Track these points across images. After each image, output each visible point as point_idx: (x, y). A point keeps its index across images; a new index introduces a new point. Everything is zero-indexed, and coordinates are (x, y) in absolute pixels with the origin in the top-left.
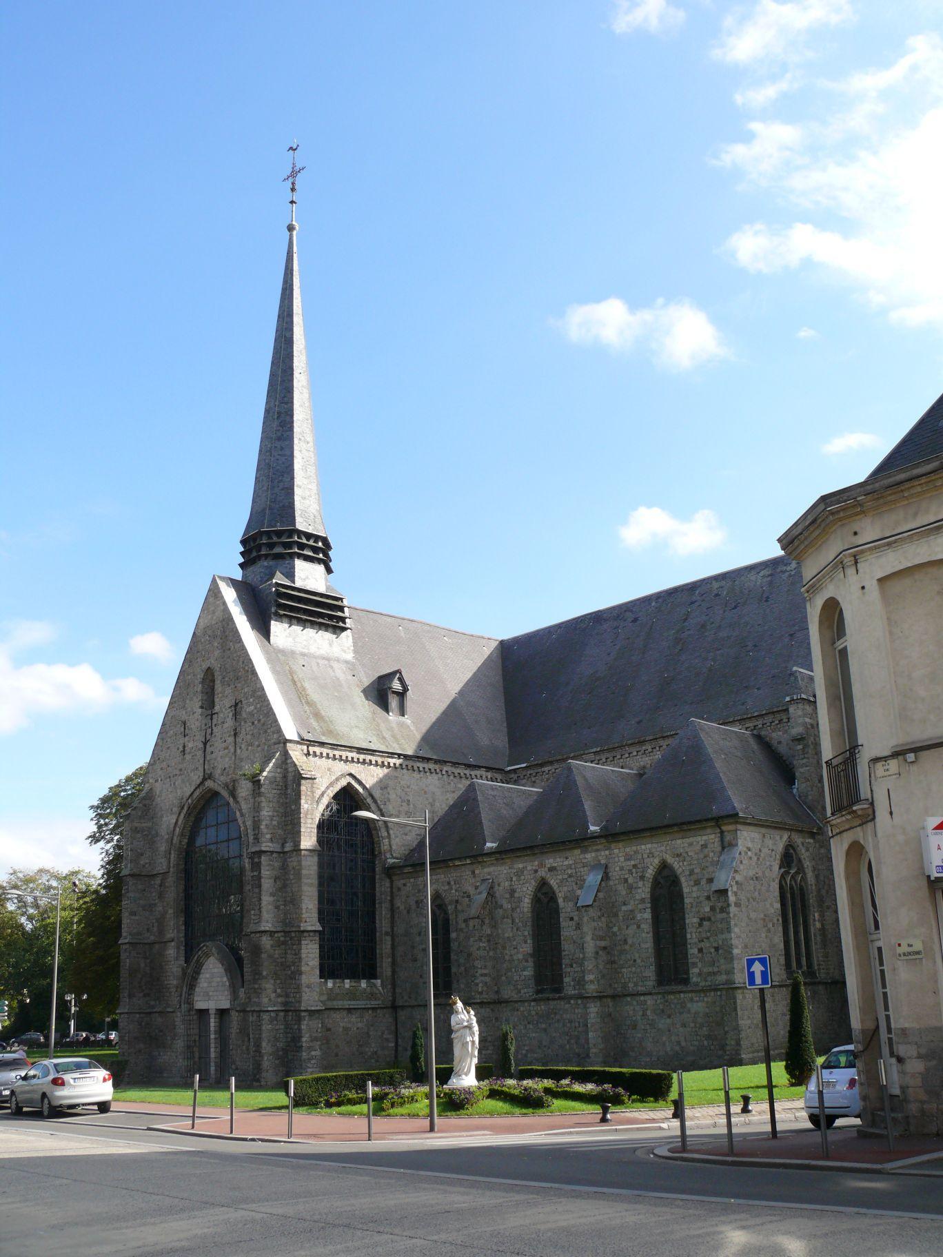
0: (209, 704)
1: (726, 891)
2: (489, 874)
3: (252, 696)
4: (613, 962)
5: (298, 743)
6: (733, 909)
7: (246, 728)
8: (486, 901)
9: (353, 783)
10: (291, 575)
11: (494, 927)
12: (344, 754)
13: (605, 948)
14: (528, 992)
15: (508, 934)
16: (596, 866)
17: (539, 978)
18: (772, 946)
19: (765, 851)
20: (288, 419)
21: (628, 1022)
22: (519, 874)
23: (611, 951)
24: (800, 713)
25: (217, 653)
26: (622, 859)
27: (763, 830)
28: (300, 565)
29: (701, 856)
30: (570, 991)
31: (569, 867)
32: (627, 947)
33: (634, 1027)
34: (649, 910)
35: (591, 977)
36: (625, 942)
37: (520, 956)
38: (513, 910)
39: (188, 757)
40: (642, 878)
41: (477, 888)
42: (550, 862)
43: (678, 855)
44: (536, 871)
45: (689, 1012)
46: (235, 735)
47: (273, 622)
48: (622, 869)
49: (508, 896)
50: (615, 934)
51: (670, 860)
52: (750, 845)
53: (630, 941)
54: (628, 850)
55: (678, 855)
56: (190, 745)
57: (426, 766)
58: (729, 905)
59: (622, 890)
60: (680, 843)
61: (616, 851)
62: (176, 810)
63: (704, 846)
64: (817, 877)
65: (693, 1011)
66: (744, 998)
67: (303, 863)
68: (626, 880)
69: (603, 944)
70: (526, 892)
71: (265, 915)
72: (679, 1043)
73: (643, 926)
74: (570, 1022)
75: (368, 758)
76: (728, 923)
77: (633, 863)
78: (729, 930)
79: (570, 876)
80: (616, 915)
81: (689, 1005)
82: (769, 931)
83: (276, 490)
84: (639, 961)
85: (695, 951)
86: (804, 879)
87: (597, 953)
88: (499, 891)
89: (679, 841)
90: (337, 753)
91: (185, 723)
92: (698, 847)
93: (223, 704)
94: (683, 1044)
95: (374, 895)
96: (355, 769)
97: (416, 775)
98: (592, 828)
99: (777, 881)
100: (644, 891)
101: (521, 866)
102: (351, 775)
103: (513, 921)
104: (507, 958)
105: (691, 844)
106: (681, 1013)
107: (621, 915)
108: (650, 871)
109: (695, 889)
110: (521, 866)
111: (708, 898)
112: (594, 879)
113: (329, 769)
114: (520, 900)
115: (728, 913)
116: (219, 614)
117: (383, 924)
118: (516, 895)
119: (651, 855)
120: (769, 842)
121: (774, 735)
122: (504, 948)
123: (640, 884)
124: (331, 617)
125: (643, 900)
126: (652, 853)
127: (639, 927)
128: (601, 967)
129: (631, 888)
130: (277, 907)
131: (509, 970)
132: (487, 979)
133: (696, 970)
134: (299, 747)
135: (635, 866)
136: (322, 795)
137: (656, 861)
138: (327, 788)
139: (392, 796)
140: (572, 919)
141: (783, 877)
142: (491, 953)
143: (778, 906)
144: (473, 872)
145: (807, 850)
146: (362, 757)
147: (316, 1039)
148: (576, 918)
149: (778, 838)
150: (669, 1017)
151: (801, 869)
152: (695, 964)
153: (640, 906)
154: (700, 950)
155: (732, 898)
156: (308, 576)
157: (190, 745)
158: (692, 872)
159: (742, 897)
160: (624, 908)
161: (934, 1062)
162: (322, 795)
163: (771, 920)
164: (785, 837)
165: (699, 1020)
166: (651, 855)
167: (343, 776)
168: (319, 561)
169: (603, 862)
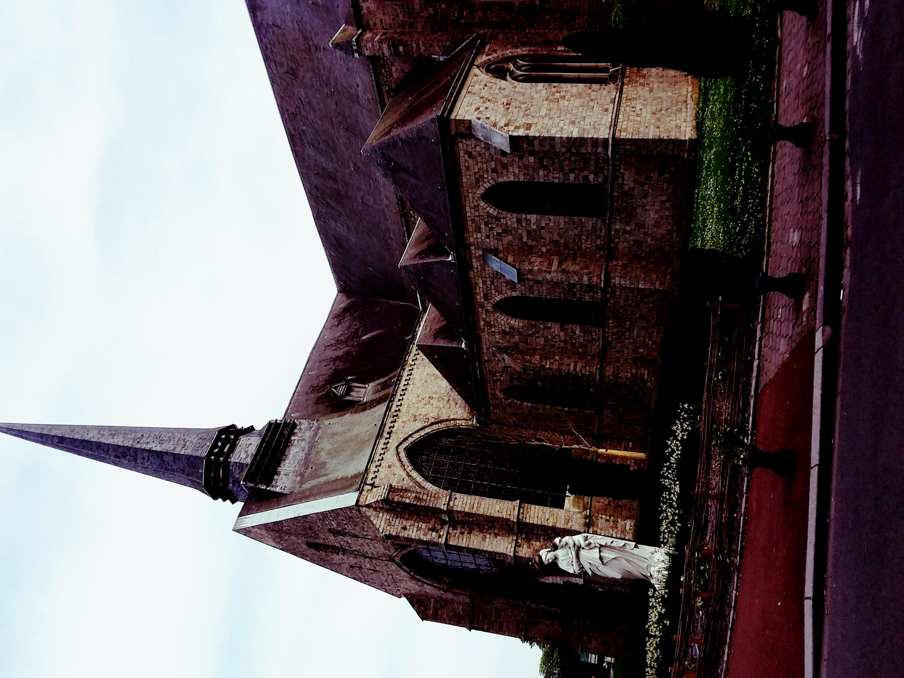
0: (336, 550)
1: (512, 138)
2: (488, 349)
3: (324, 521)
5: (360, 493)
6: (532, 133)
7: (349, 528)
8: (511, 356)
9: (401, 449)
10: (241, 466)
12: (380, 451)
14: (596, 333)
15: (542, 341)
16: (484, 259)
18: (580, 95)
19: (484, 93)
20: (121, 450)
22: (488, 324)
23: (563, 251)
24: (369, 45)
25: (293, 538)
26: (479, 235)
27: (464, 92)
28: (234, 459)
29: (479, 158)
31: (484, 283)
32: (562, 241)
33: (638, 243)
34: (529, 216)
35: (585, 278)
36: (557, 242)
37: (562, 334)
38: (520, 334)
39: (377, 568)
40: (498, 219)
41: (499, 360)
42: (480, 298)
43: (478, 182)
44: (487, 311)
45: (633, 189)
46: (357, 536)
48: (488, 237)
49: (508, 337)
50: (548, 251)
51: (481, 191)
52: (474, 107)
53: (556, 238)
54: (470, 229)
55: (478, 182)
56: (368, 566)
57: (404, 379)
58: (527, 137)
59: (508, 238)
60: (466, 179)
61: (472, 240)
62: (420, 583)
63: (470, 155)
64: (524, 44)
65: (632, 185)
66: (625, 130)
67: (459, 509)
68: (499, 234)
70: (504, 321)
71: (501, 549)
72: (663, 202)
73: (543, 224)
74: (627, 299)
75: (387, 429)
76: (545, 138)
77: (483, 226)
78: (552, 139)
79: (493, 283)
80: (531, 247)
81: (626, 188)
82: (563, 97)
83: (175, 467)
84: (576, 232)
85: (572, 176)
86: (522, 57)
88: (503, 343)
89: (464, 180)
90: (377, 457)
91: (351, 566)
92: (471, 161)
93: (332, 540)
94: (664, 198)
96: (393, 442)
97: (410, 388)
98: (450, 259)
99: (516, 83)
100: (510, 219)
101: (482, 323)
102: (397, 447)
103: (530, 335)
104: (562, 345)
105: (468, 168)
106: (633, 197)
107: (530, 242)
108: (491, 211)
109: (511, 170)
110: (482, 323)
111: (521, 158)
112: (495, 264)
113: (389, 467)
114: (512, 327)
115: (535, 137)
116: (264, 532)
118: (507, 330)
119: (476, 208)
120: (478, 87)
121: (395, 75)
122: (554, 346)
123: (503, 221)
124: (282, 435)
125: (519, 221)
126: (476, 207)
127: (543, 228)
129: (506, 231)
130: (496, 535)
131: (573, 345)
133: (591, 177)
134: (364, 493)
135: (486, 224)
136: (409, 476)
137: (482, 204)
138: (405, 470)
139: (423, 411)
141: (516, 79)
143: (540, 85)
144: (487, 361)
145: (495, 51)
146: (385, 435)
147: (615, 522)
148: (531, 283)
149: (475, 78)
150: (635, 209)
151: (512, 59)
152: (586, 178)
154: (572, 171)
155: (521, 132)
156: (245, 451)
157: (368, 566)
158: (494, 171)
159: (521, 121)
160: (525, 239)
162: (409, 476)
163: (553, 94)
164: (475, 70)
165: (642, 180)
166: (476, 208)
167: (398, 454)
168: (236, 439)
169: (481, 253)
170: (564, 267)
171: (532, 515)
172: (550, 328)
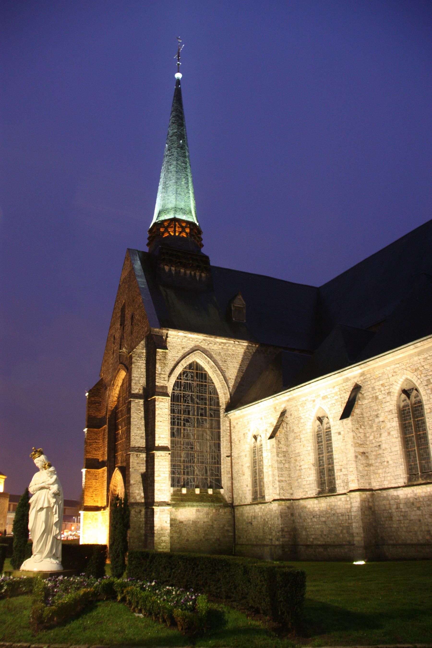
4: (369, 465)
11: (288, 446)
13: (364, 453)
17: (321, 483)
21: (386, 515)
30: (340, 489)
32: (381, 452)
47: (245, 344)
53: (383, 446)
69: (362, 450)
73: (392, 433)
77: (381, 382)
84: (391, 462)
87: (356, 457)
93: (128, 316)
95: (219, 433)
117: (224, 452)
123: (388, 398)
127: (389, 433)
128: (361, 468)
132: (284, 484)
135: (382, 385)
140: (339, 433)
142: (287, 465)
153: (389, 417)
161: (281, 625)
170: (359, 457)
171: (161, 464)
172: (309, 454)
